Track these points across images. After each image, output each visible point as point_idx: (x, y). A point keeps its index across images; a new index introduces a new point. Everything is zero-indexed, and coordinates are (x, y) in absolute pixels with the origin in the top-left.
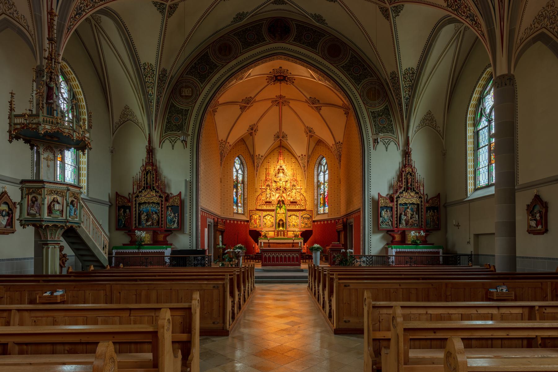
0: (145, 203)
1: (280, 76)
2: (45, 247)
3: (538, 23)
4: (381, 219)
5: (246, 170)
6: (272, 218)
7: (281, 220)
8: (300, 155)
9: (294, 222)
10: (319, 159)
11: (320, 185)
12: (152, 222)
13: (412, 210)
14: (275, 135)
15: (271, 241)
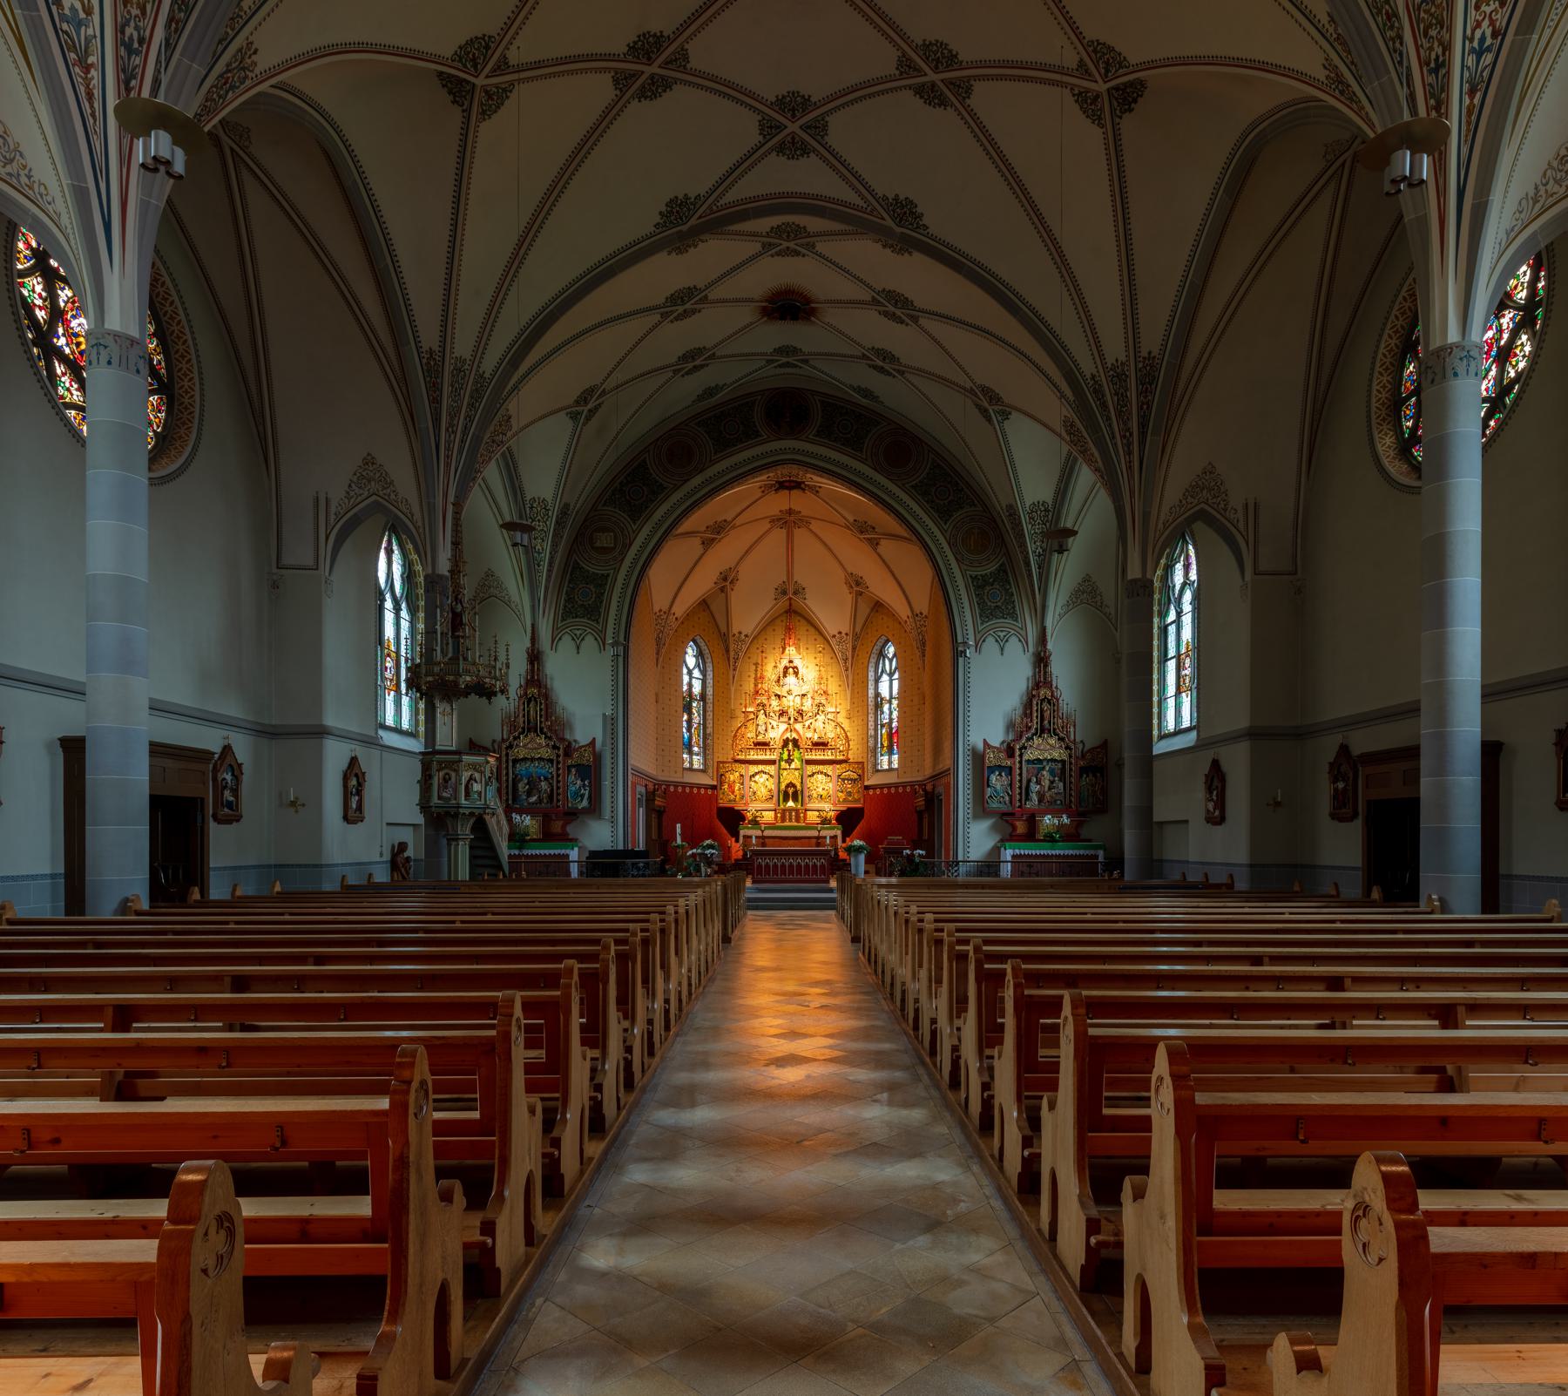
0: (525, 759)
1: (789, 481)
2: (454, 843)
3: (1192, 496)
4: (989, 791)
5: (709, 669)
7: (791, 785)
8: (836, 633)
10: (879, 644)
12: (539, 797)
13: (1052, 772)
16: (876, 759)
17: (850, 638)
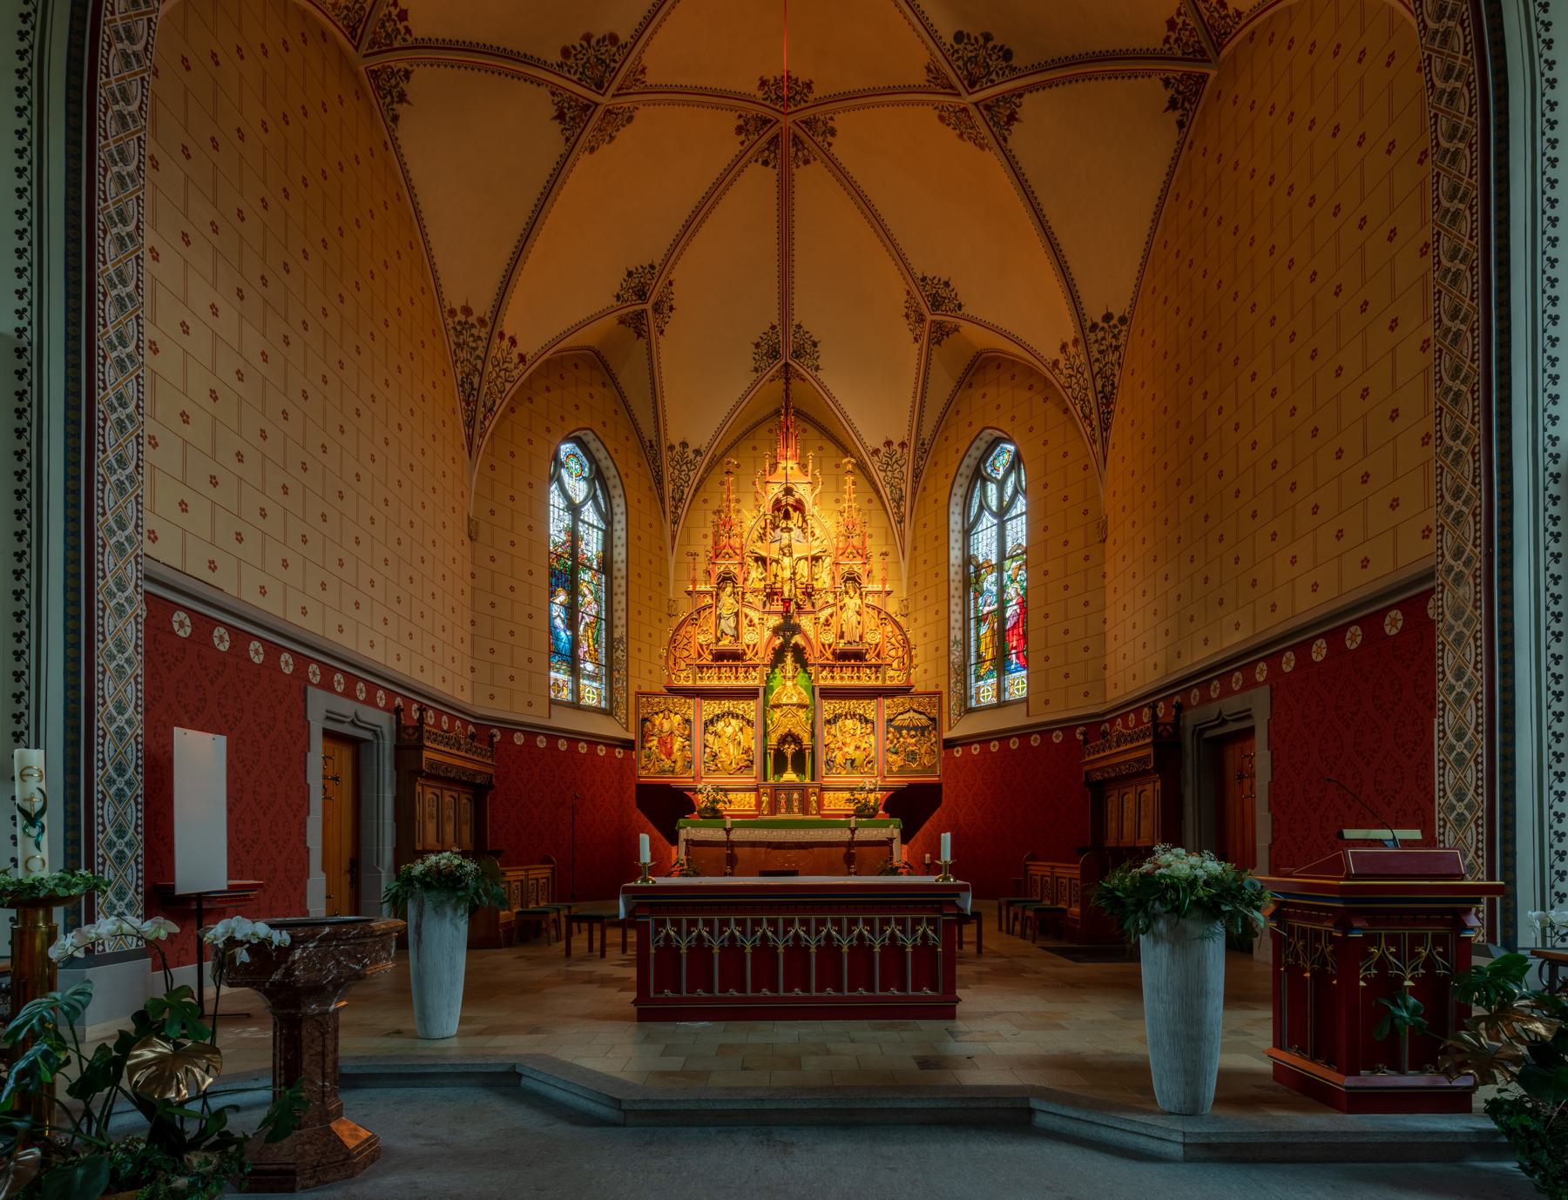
5: (619, 509)
6: (749, 731)
8: (878, 443)
9: (850, 749)
10: (975, 453)
11: (978, 576)
15: (738, 835)
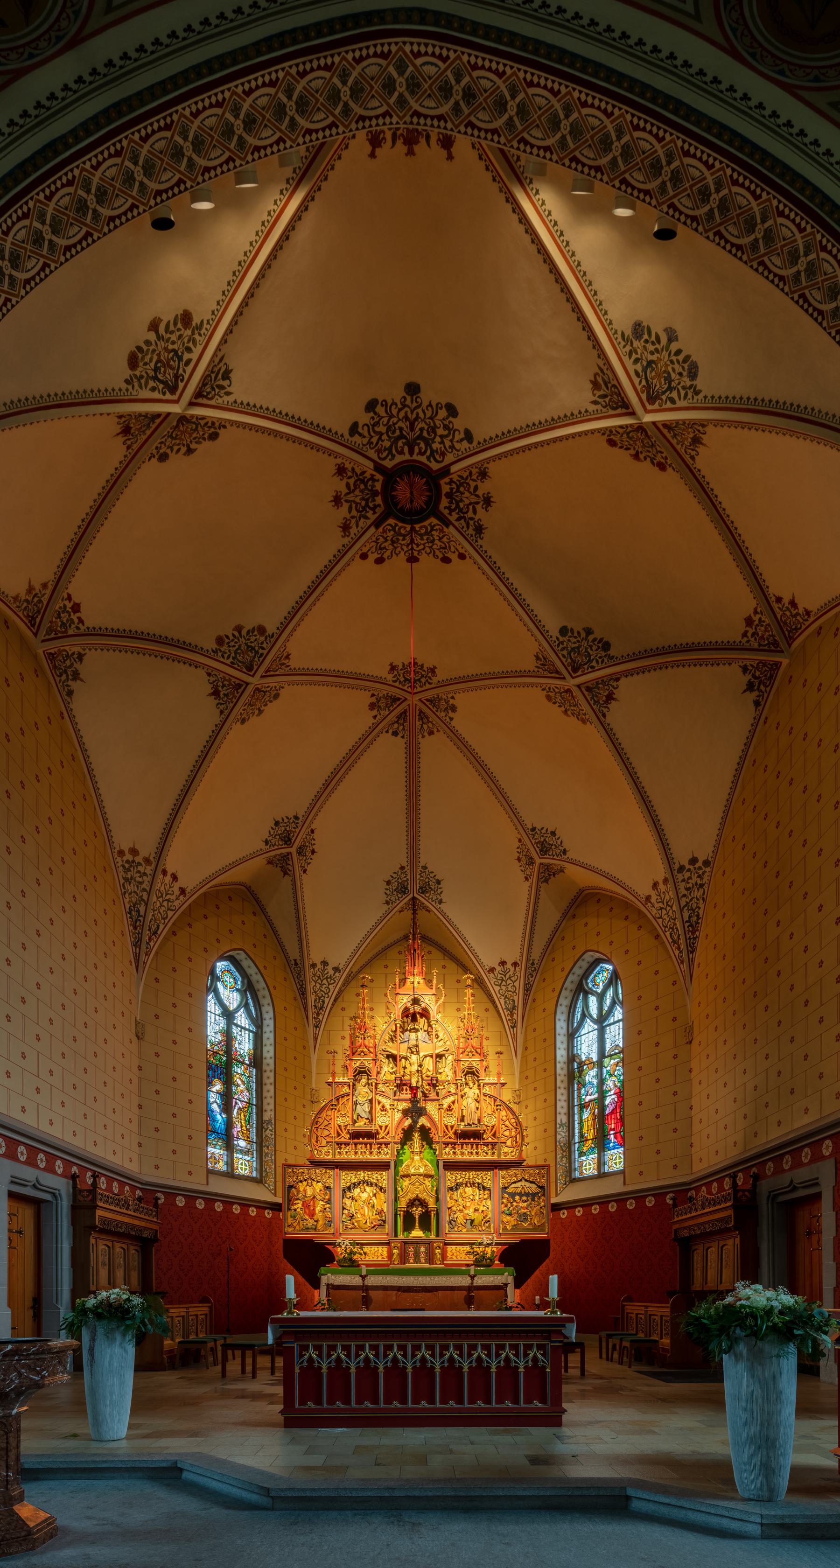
6: (382, 1196)
9: (470, 1212)
10: (578, 971)
11: (581, 1071)
14: (388, 883)
16: (570, 1161)
17: (521, 971)
